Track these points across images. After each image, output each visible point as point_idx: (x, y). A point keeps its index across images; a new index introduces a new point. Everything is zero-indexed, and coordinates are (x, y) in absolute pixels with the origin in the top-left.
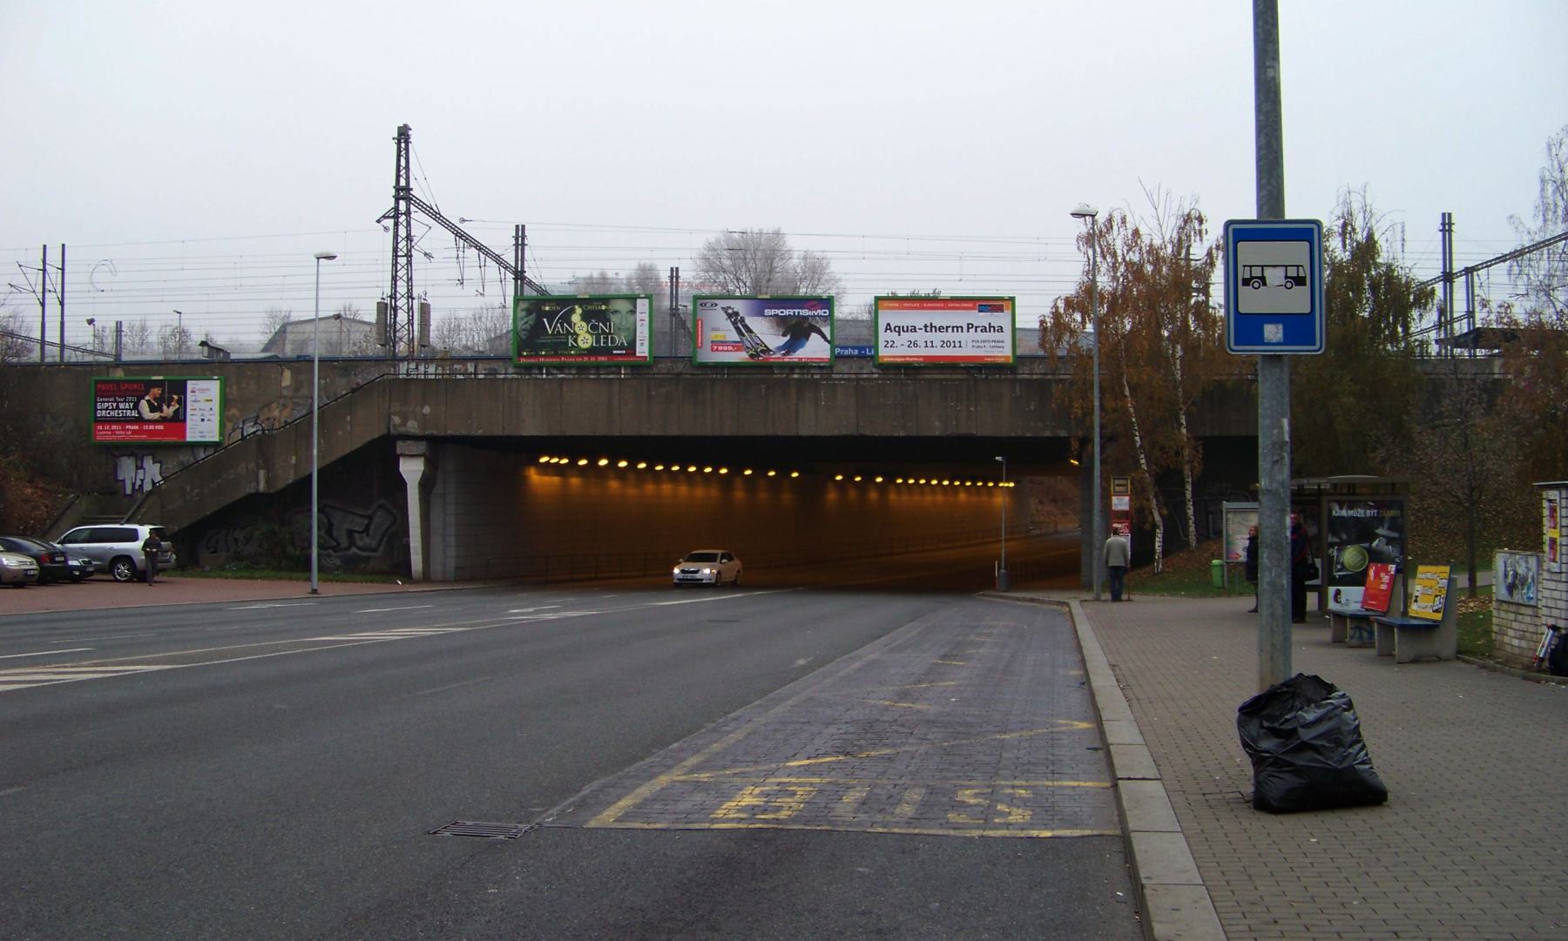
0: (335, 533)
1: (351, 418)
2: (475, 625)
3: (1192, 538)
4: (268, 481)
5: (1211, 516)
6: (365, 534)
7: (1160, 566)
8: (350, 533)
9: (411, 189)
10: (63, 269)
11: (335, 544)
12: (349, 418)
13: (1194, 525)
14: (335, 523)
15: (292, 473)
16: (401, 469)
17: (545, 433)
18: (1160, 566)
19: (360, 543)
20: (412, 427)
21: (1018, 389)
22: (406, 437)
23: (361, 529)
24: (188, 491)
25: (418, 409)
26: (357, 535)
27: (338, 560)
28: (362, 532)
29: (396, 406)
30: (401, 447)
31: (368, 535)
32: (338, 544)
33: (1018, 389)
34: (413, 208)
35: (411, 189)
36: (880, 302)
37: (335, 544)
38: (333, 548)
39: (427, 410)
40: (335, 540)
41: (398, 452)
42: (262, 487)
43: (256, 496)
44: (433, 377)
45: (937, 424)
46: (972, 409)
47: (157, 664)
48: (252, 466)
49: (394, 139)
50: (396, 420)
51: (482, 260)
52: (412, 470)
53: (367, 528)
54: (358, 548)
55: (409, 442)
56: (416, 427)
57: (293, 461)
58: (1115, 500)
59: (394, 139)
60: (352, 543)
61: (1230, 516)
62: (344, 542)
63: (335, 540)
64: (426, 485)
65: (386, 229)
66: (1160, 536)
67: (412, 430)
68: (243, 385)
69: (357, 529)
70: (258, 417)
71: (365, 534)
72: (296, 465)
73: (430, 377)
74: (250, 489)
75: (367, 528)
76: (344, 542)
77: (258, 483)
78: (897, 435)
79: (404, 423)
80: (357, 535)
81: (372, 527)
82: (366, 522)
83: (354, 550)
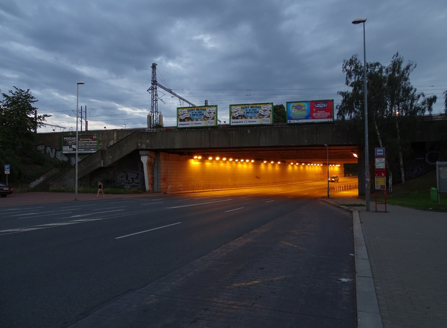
0: (128, 178)
1: (127, 144)
2: (105, 217)
3: (403, 180)
4: (104, 164)
5: (407, 171)
6: (137, 179)
7: (391, 190)
8: (133, 178)
9: (157, 81)
10: (86, 112)
11: (128, 182)
12: (126, 144)
13: (404, 174)
14: (128, 175)
15: (110, 161)
16: (141, 159)
18: (391, 190)
19: (135, 181)
20: (144, 146)
21: (334, 128)
22: (142, 150)
23: (135, 177)
24: (82, 167)
25: (145, 141)
26: (134, 179)
27: (129, 186)
28: (135, 178)
29: (139, 141)
30: (141, 153)
31: (137, 179)
32: (129, 182)
33: (334, 128)
34: (157, 87)
35: (157, 81)
36: (288, 104)
37: (128, 182)
38: (128, 183)
39: (148, 141)
40: (129, 181)
41: (140, 154)
42: (102, 166)
43: (101, 168)
44: (147, 131)
45: (306, 141)
46: (318, 136)
47: (76, 217)
48: (100, 159)
49: (151, 67)
50: (139, 144)
51: (180, 100)
52: (144, 159)
53: (137, 178)
54: (135, 183)
55: (143, 151)
56: (145, 146)
57: (111, 158)
58: (377, 160)
59: (151, 67)
60: (133, 182)
61: (441, 169)
62: (131, 181)
63: (129, 181)
64: (149, 164)
65: (150, 93)
66: (391, 178)
67: (144, 148)
68: (103, 136)
69: (134, 177)
70: (107, 145)
71: (137, 179)
72: (111, 158)
73: (154, 131)
74: (99, 166)
75: (137, 178)
76: (131, 181)
77: (101, 164)
78: (292, 145)
79: (141, 146)
80: (134, 179)
81: (139, 177)
82: (137, 175)
83: (134, 183)
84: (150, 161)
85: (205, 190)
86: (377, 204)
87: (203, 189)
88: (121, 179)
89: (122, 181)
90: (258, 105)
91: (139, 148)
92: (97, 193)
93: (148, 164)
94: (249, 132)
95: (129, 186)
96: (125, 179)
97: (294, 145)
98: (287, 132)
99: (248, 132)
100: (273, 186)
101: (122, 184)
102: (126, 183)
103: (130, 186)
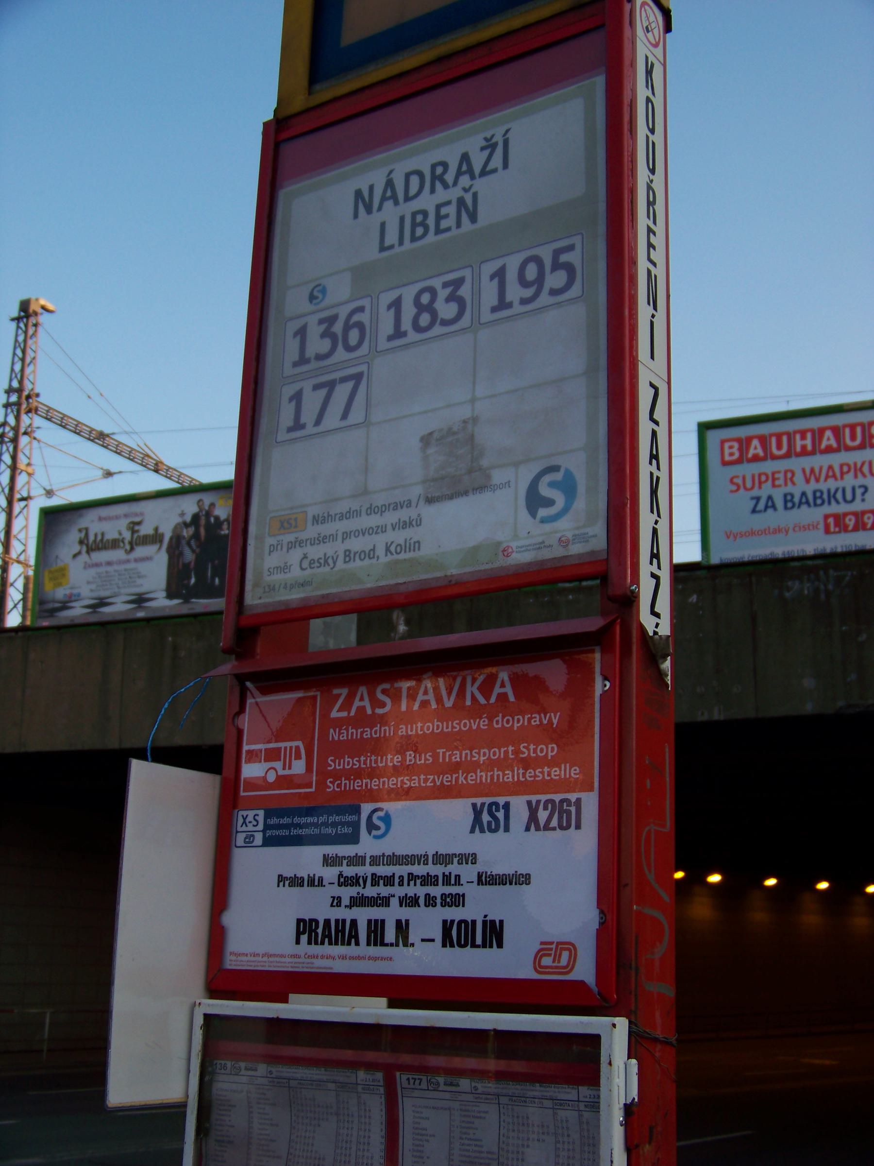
45: (809, 683)
78: (705, 717)
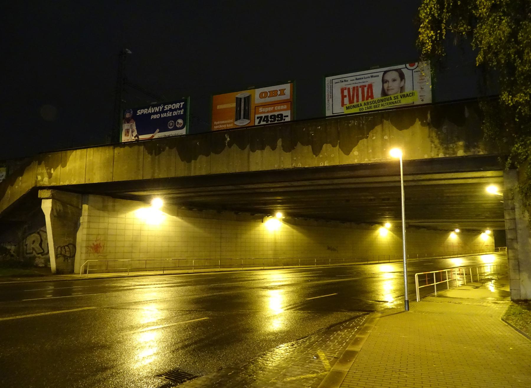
0: (43, 245)
17: (105, 181)
32: (44, 251)
52: (47, 206)
64: (56, 216)
78: (322, 165)
84: (60, 210)
85: (451, 257)
86: (411, 71)
87: (162, 269)
88: (32, 246)
89: (33, 249)
90: (411, 179)
91: (38, 185)
92: (89, 266)
93: (55, 216)
94: (228, 139)
95: (42, 259)
96: (38, 245)
97: (326, 165)
98: (311, 133)
99: (226, 139)
100: (458, 257)
101: (33, 255)
102: (38, 254)
103: (44, 258)
